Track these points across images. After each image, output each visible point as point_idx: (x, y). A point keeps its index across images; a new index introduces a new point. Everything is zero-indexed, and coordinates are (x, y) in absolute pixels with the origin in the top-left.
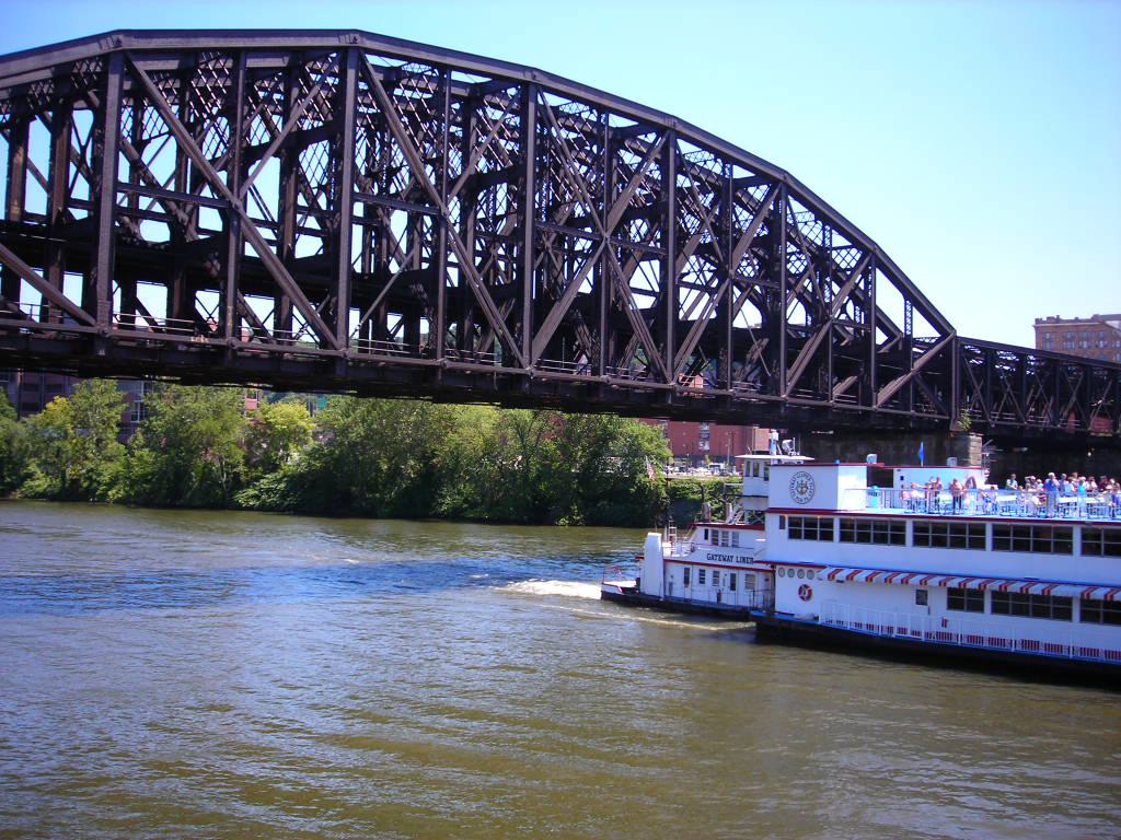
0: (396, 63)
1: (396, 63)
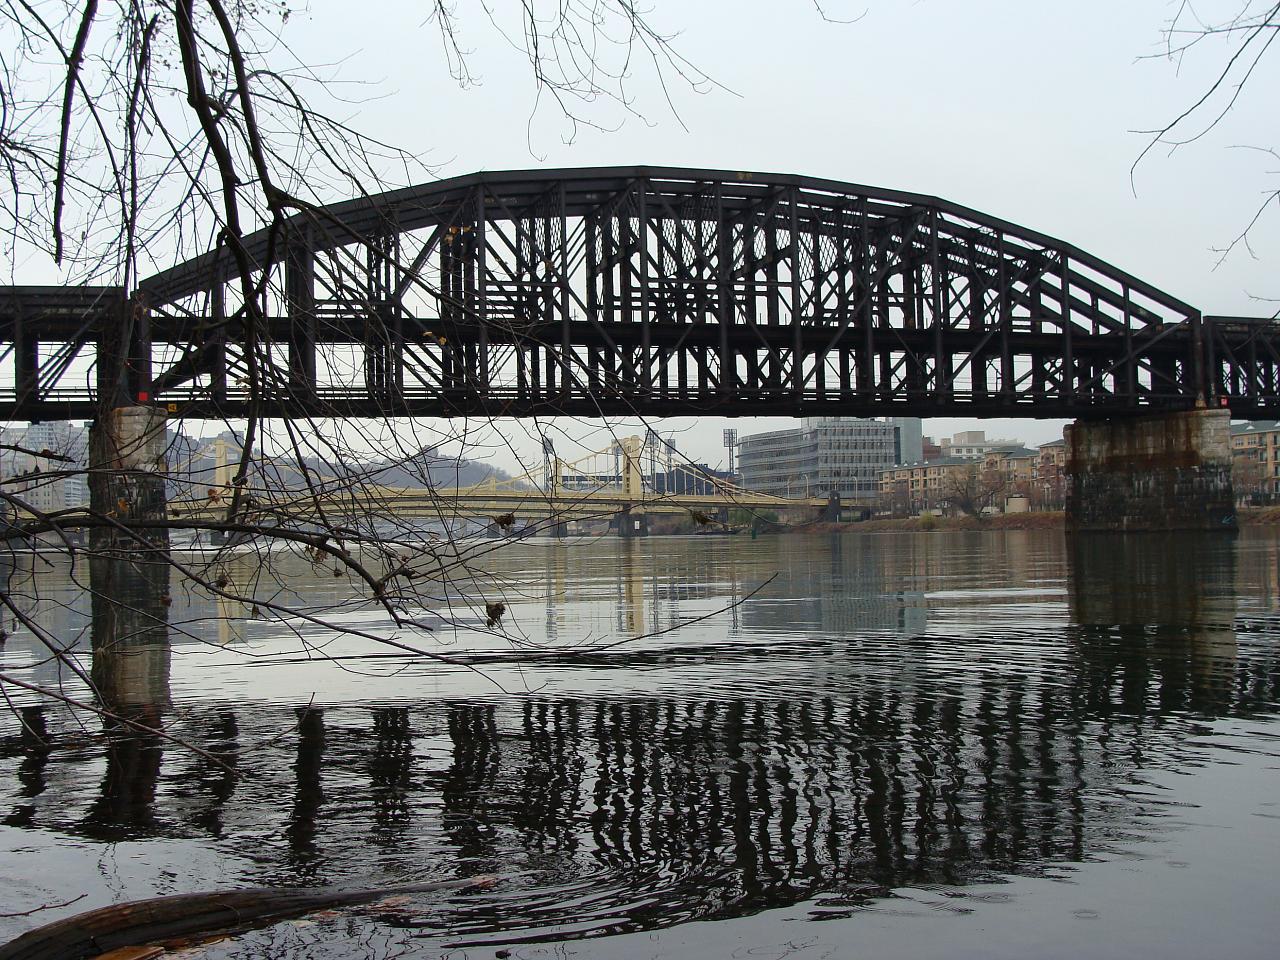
0: (975, 226)
1: (975, 226)
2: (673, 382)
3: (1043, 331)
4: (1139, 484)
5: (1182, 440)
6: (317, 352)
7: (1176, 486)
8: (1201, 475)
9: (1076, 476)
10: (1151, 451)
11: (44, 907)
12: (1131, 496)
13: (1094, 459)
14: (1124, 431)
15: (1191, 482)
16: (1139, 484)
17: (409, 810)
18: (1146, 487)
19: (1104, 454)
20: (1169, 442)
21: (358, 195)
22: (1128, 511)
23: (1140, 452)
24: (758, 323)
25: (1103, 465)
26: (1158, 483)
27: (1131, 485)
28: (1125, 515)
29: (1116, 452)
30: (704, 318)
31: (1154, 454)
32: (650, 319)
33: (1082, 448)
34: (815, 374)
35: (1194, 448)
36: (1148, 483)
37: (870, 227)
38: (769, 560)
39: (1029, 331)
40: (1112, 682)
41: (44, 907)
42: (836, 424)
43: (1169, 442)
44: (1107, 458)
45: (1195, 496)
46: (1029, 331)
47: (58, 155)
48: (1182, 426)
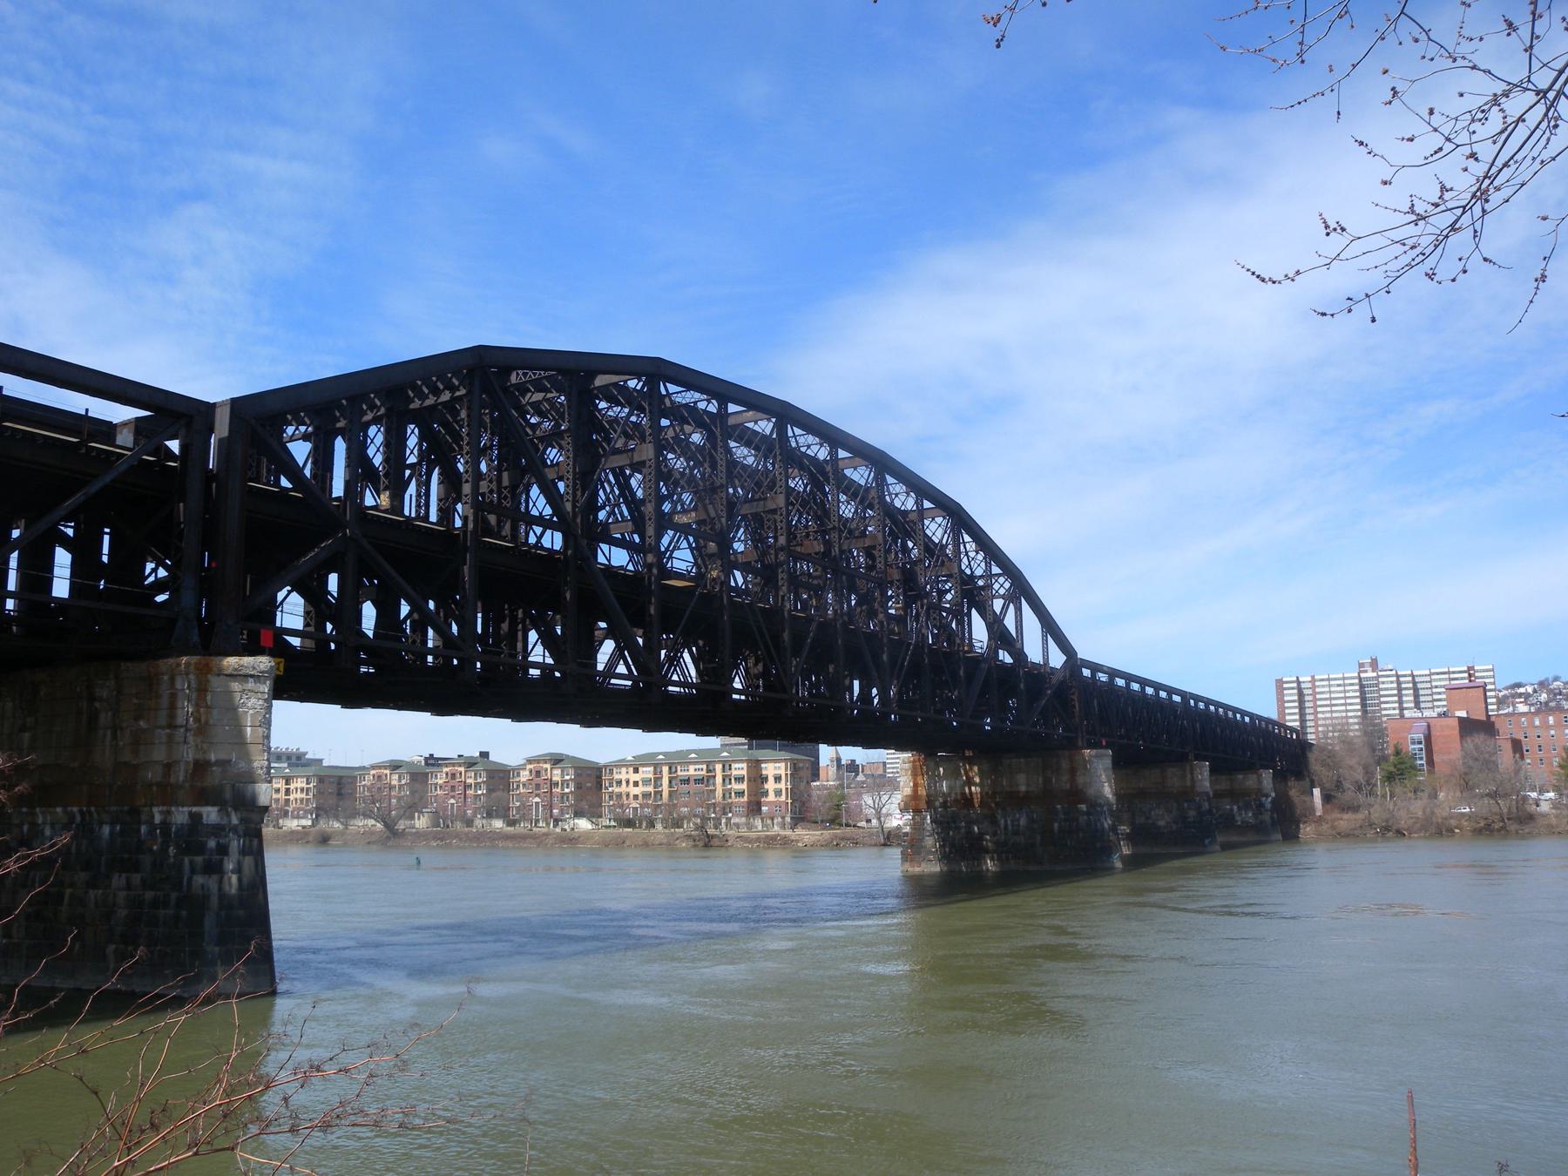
3: (53, 595)
4: (1006, 821)
5: (1065, 778)
7: (1056, 825)
8: (1088, 813)
10: (1023, 788)
11: (1520, 321)
16: (1006, 821)
18: (839, 598)
21: (1274, 715)
23: (1008, 789)
24: (278, 624)
30: (704, 645)
31: (1027, 792)
32: (329, 632)
34: (1014, 633)
35: (1080, 787)
36: (1018, 820)
39: (334, 601)
40: (883, 652)
41: (1520, 321)
45: (1081, 835)
46: (334, 601)
48: (1065, 764)
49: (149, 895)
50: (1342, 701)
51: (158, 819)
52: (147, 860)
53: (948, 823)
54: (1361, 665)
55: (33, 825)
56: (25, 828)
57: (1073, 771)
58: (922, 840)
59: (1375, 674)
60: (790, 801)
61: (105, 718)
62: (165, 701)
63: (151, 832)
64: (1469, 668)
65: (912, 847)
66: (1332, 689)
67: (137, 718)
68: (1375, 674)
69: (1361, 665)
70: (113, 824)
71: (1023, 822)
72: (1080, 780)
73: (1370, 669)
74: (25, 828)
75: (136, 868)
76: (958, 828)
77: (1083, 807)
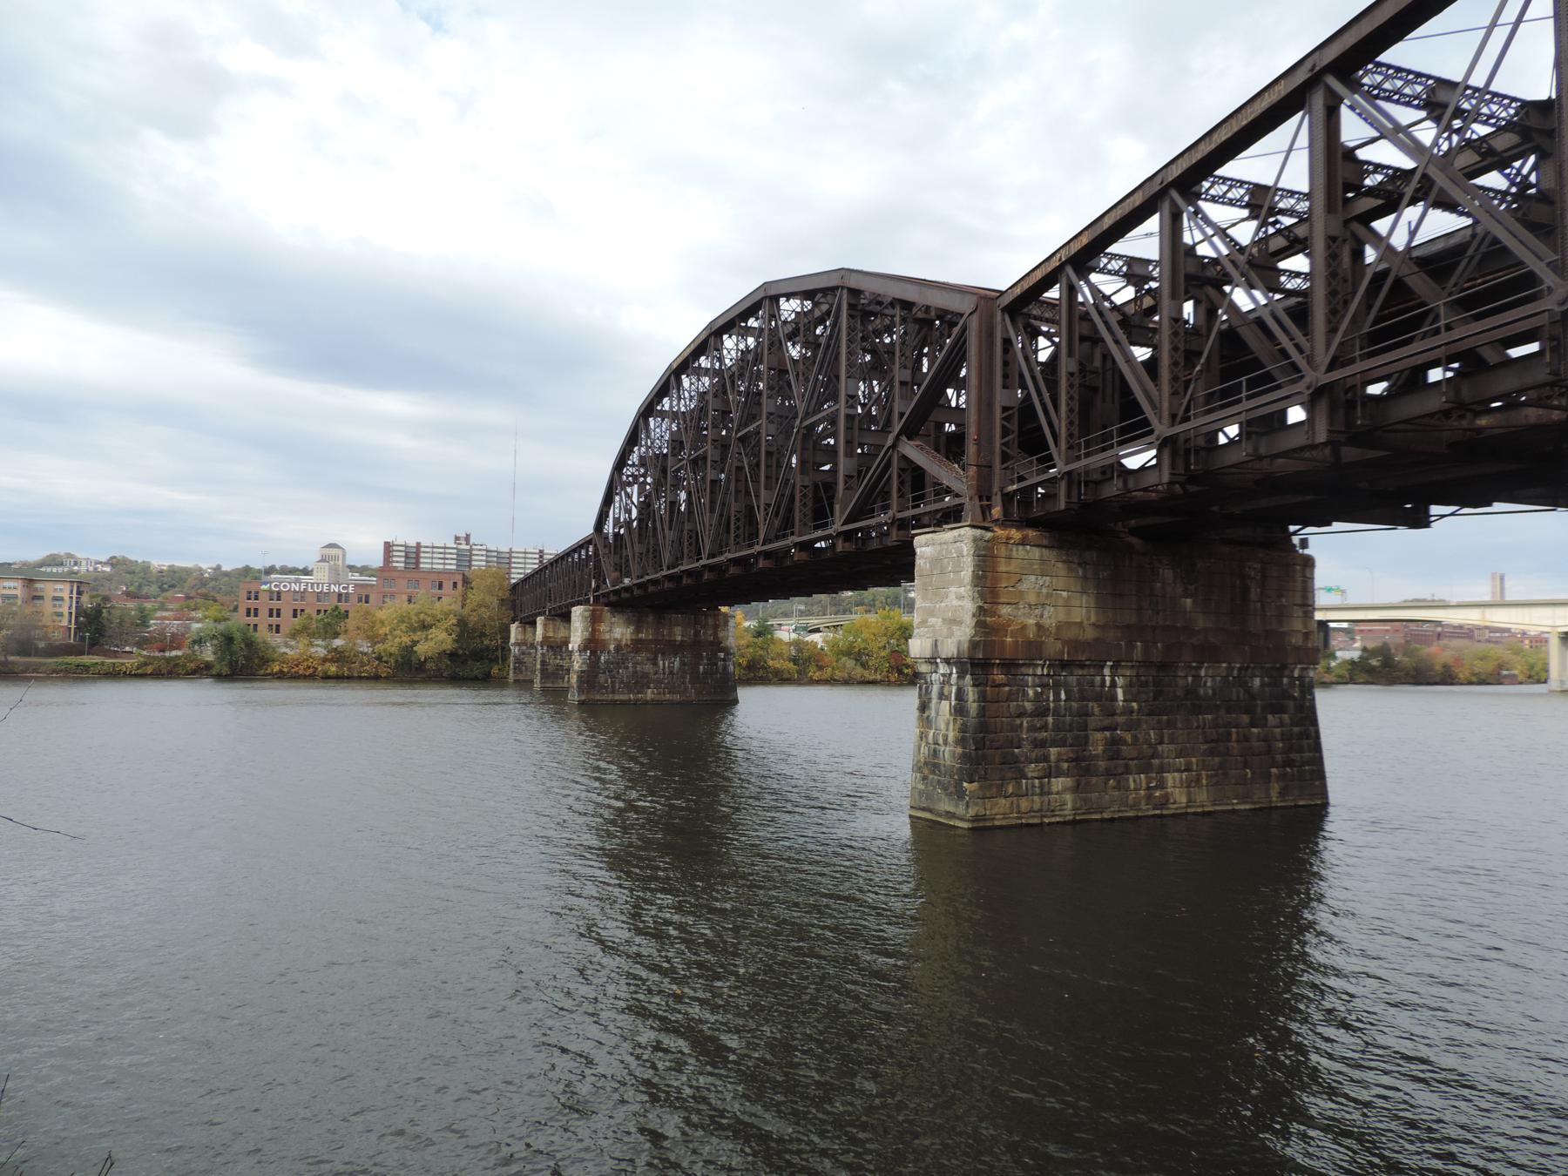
2: (395, 559)
4: (664, 664)
6: (1457, 508)
8: (724, 660)
9: (593, 653)
10: (679, 638)
12: (655, 674)
13: (616, 640)
14: (650, 618)
15: (716, 664)
16: (664, 664)
17: (1296, 1127)
19: (628, 637)
20: (697, 633)
22: (652, 685)
23: (667, 638)
25: (626, 645)
26: (683, 664)
27: (655, 664)
28: (649, 688)
29: (642, 636)
33: (603, 627)
37: (715, 411)
38: (467, 701)
42: (887, 622)
43: (697, 633)
44: (632, 640)
47: (1477, 80)
49: (1296, 729)
50: (447, 561)
51: (1296, 674)
52: (1291, 704)
53: (618, 663)
54: (457, 538)
55: (1197, 677)
56: (1190, 679)
57: (716, 627)
58: (596, 676)
59: (468, 547)
60: (73, 626)
61: (1254, 593)
62: (1299, 585)
63: (1292, 685)
64: (541, 551)
65: (588, 682)
66: (435, 555)
67: (1280, 596)
68: (468, 547)
69: (457, 538)
70: (1262, 677)
71: (677, 664)
72: (721, 634)
73: (464, 542)
74: (1190, 679)
75: (1283, 710)
76: (627, 668)
77: (722, 655)
